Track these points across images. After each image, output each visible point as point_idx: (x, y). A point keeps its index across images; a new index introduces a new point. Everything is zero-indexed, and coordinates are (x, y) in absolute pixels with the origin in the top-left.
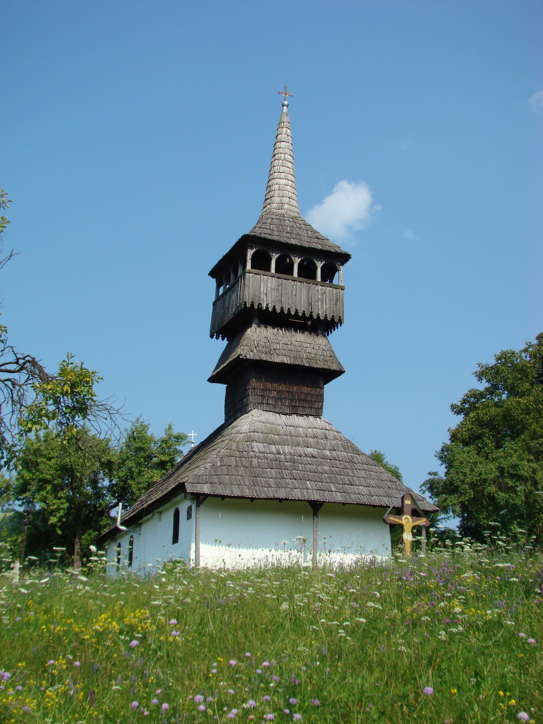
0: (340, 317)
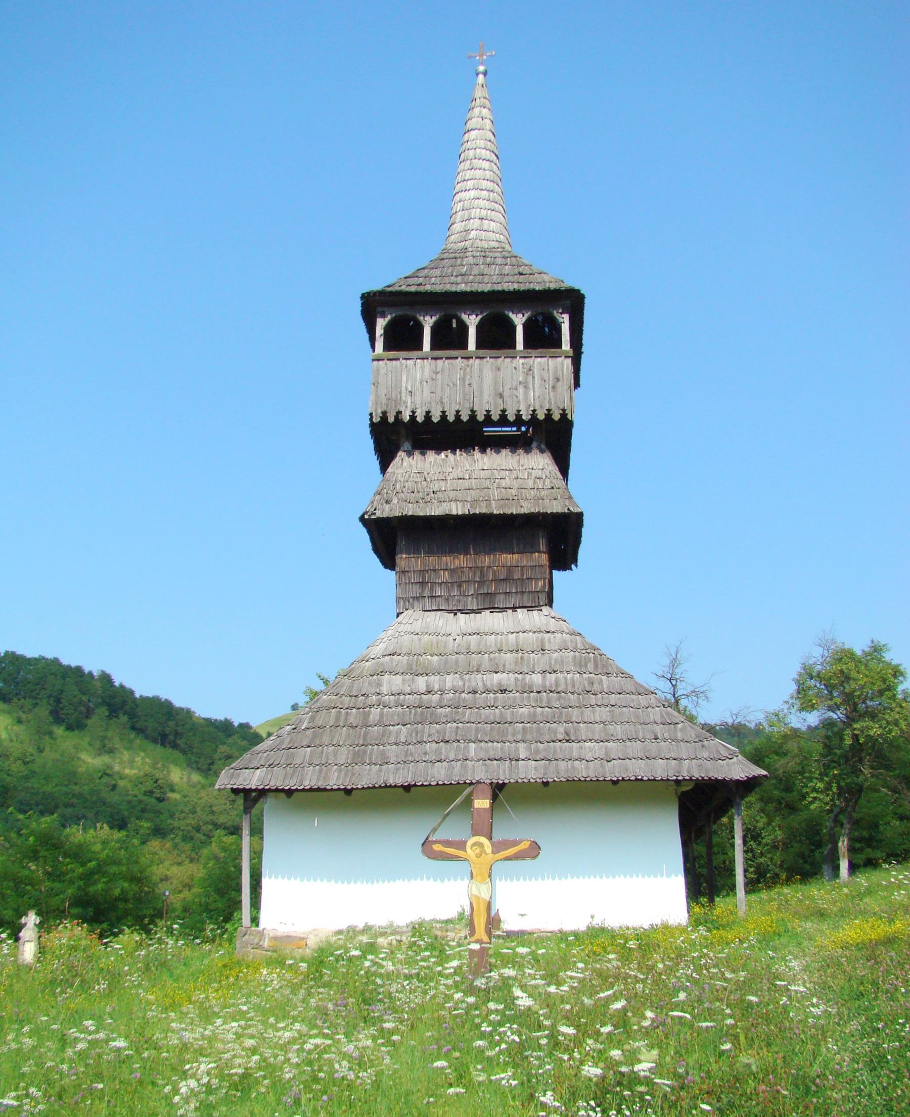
0: (564, 410)
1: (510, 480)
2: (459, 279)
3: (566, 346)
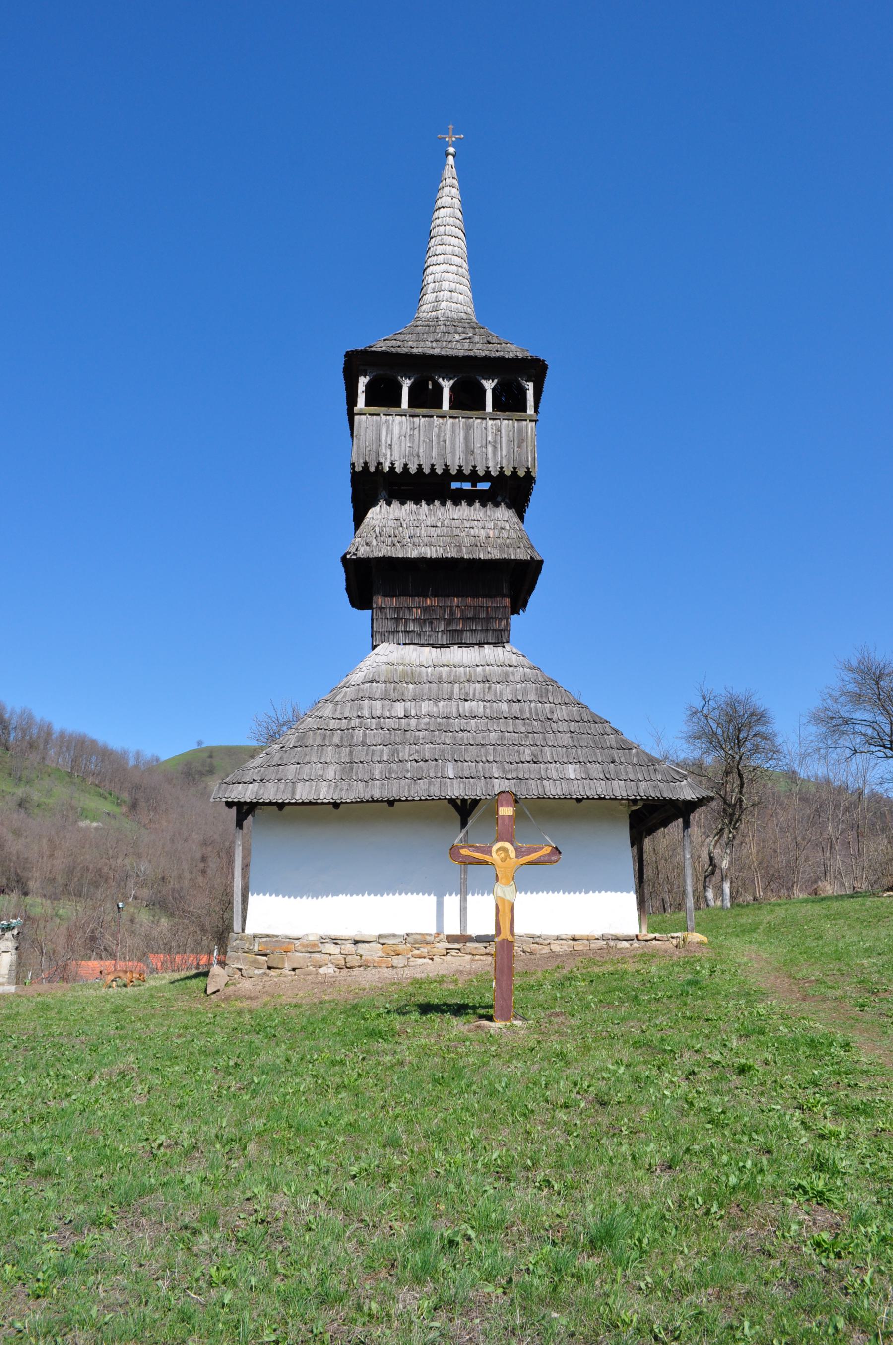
0: (528, 468)
1: (477, 531)
2: (434, 344)
3: (530, 411)
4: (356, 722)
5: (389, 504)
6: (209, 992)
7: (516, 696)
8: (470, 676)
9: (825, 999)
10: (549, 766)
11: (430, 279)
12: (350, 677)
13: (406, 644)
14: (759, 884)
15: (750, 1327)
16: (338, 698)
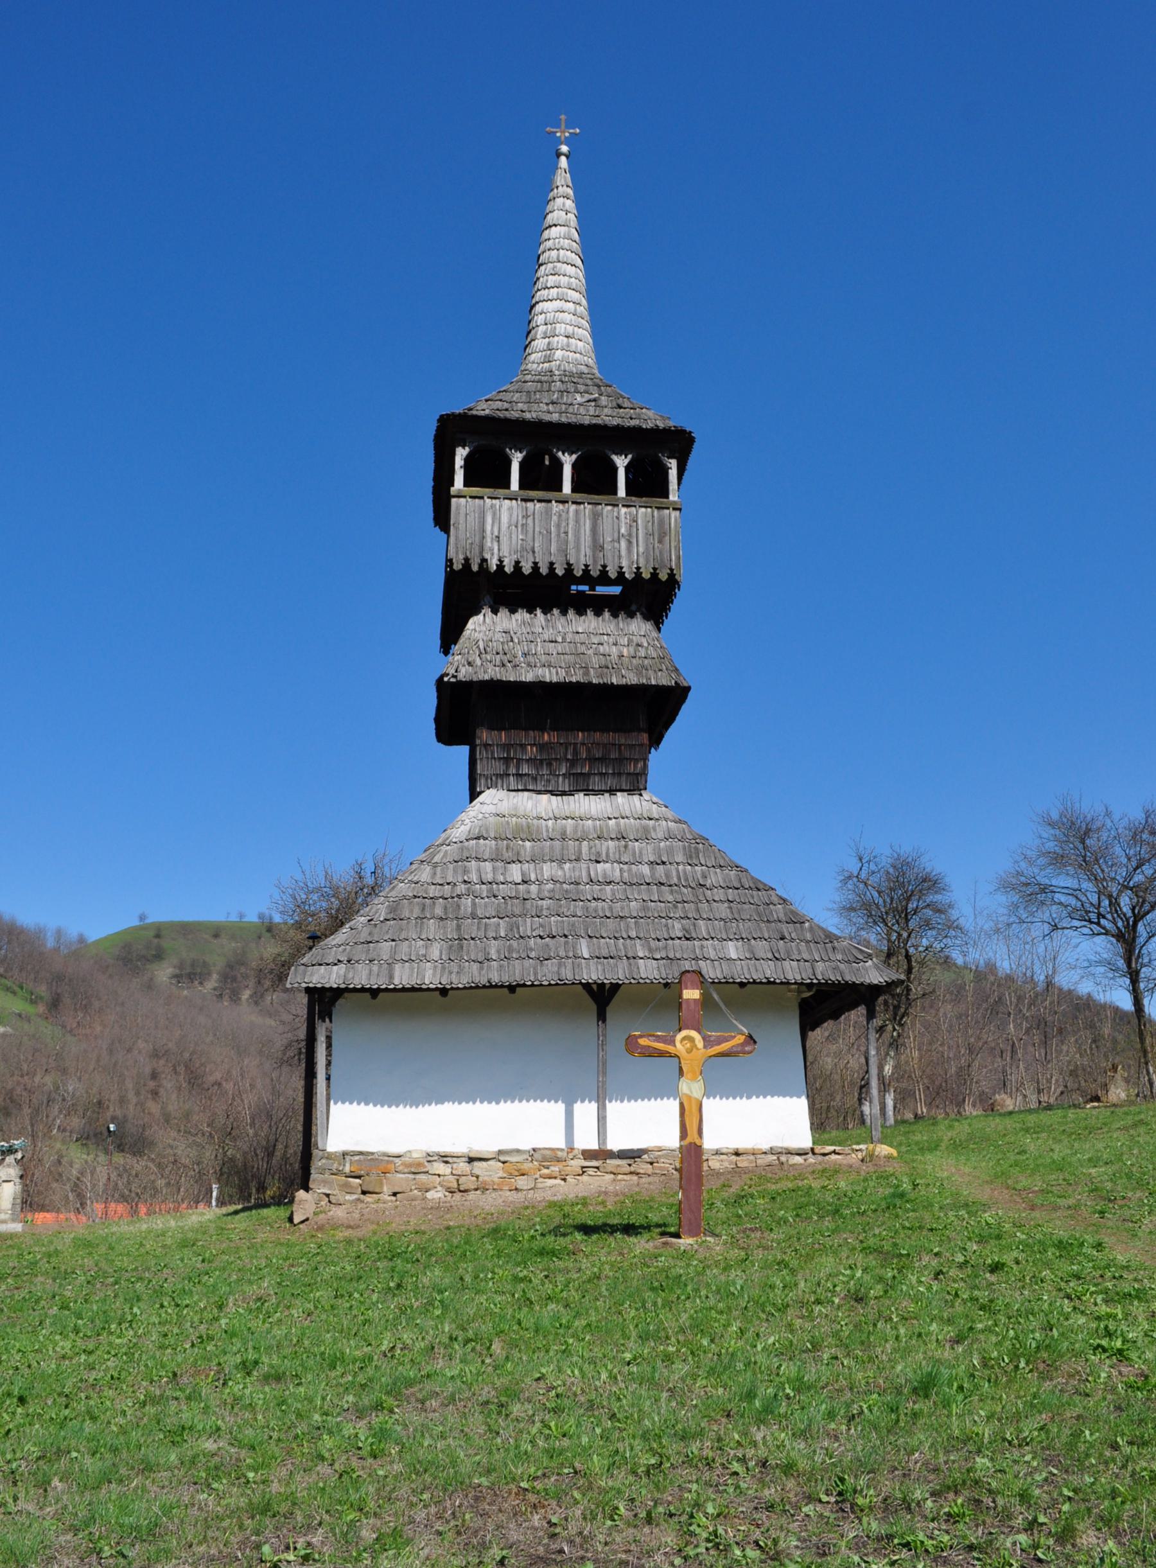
0: (672, 570)
2: (551, 407)
4: (461, 888)
5: (495, 612)
6: (296, 1221)
7: (660, 856)
8: (602, 832)
9: (1056, 1208)
10: (705, 943)
11: (540, 319)
12: (449, 831)
13: (518, 790)
14: (921, 1095)
15: (1091, 1435)
16: (437, 859)
